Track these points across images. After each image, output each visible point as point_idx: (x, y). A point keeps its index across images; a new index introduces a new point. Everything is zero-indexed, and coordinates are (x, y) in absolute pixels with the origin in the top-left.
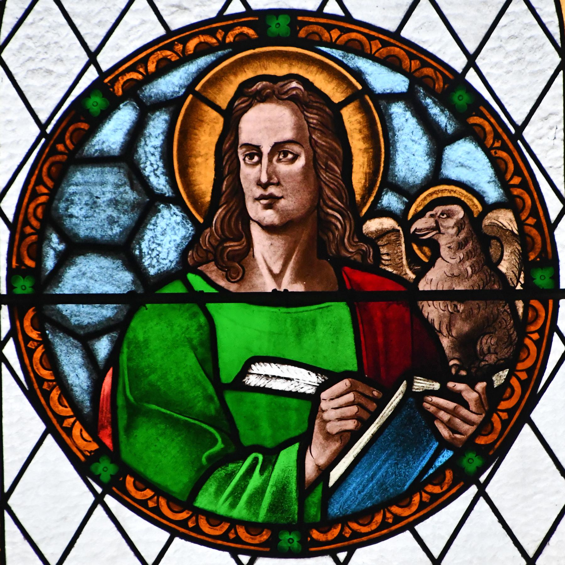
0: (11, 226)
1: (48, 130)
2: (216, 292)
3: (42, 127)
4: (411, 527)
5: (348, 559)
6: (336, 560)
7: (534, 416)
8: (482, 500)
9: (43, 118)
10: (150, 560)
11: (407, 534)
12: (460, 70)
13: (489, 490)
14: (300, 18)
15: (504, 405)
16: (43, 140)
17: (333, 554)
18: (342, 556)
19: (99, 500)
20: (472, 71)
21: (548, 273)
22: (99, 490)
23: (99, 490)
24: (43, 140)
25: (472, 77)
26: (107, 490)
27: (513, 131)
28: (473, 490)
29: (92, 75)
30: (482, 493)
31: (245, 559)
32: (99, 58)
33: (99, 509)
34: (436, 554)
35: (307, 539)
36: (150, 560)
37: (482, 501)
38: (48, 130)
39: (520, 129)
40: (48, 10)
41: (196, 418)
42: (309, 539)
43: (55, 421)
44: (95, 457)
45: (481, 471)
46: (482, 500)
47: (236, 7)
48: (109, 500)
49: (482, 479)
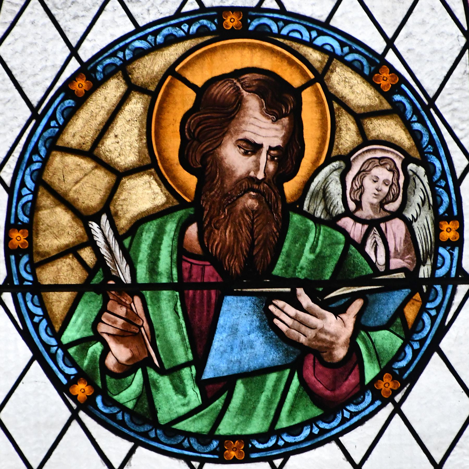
0: (9, 190)
1: (39, 112)
2: (227, 392)
3: (34, 110)
4: (336, 439)
5: (283, 464)
6: (272, 465)
7: (443, 345)
8: (397, 416)
9: (35, 104)
10: (116, 464)
11: (333, 445)
12: (380, 52)
13: (404, 408)
14: (216, 457)
15: (418, 337)
16: (34, 122)
17: (270, 460)
18: (277, 462)
19: (74, 416)
20: (391, 51)
21: (454, 225)
22: (74, 406)
23: (74, 406)
24: (34, 122)
25: (391, 57)
26: (82, 406)
27: (427, 103)
28: (390, 407)
29: (74, 65)
30: (397, 410)
31: (196, 464)
32: (80, 52)
33: (75, 423)
34: (357, 461)
35: (249, 446)
36: (116, 464)
37: (397, 417)
38: (39, 112)
39: (432, 101)
40: (35, 4)
41: (142, 339)
42: (250, 446)
43: (41, 348)
44: (73, 381)
45: (395, 392)
46: (397, 416)
47: (191, 5)
48: (82, 414)
49: (398, 398)
